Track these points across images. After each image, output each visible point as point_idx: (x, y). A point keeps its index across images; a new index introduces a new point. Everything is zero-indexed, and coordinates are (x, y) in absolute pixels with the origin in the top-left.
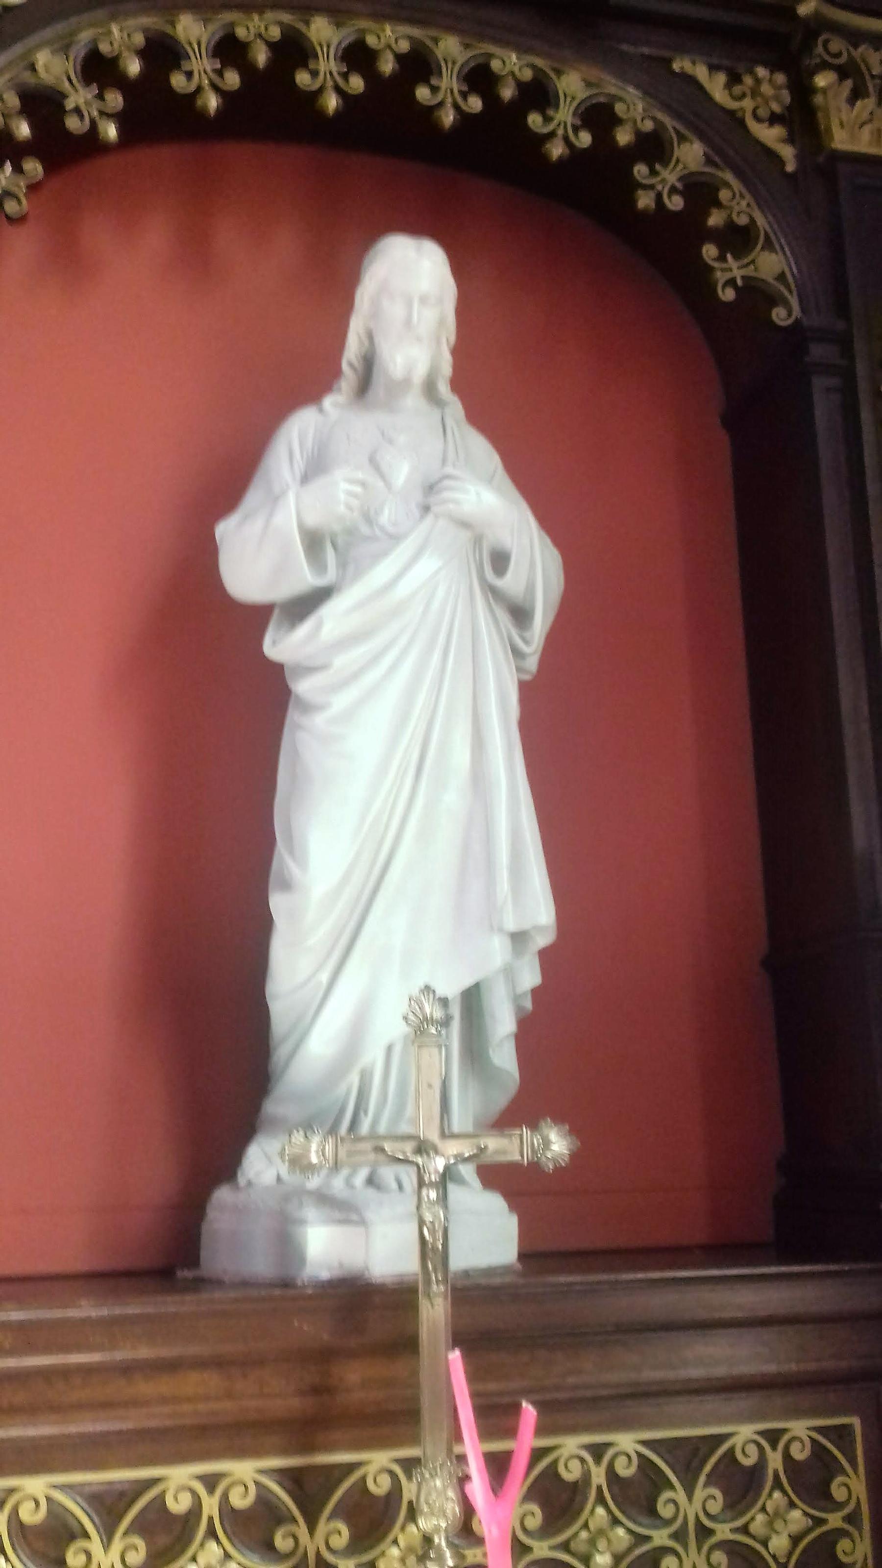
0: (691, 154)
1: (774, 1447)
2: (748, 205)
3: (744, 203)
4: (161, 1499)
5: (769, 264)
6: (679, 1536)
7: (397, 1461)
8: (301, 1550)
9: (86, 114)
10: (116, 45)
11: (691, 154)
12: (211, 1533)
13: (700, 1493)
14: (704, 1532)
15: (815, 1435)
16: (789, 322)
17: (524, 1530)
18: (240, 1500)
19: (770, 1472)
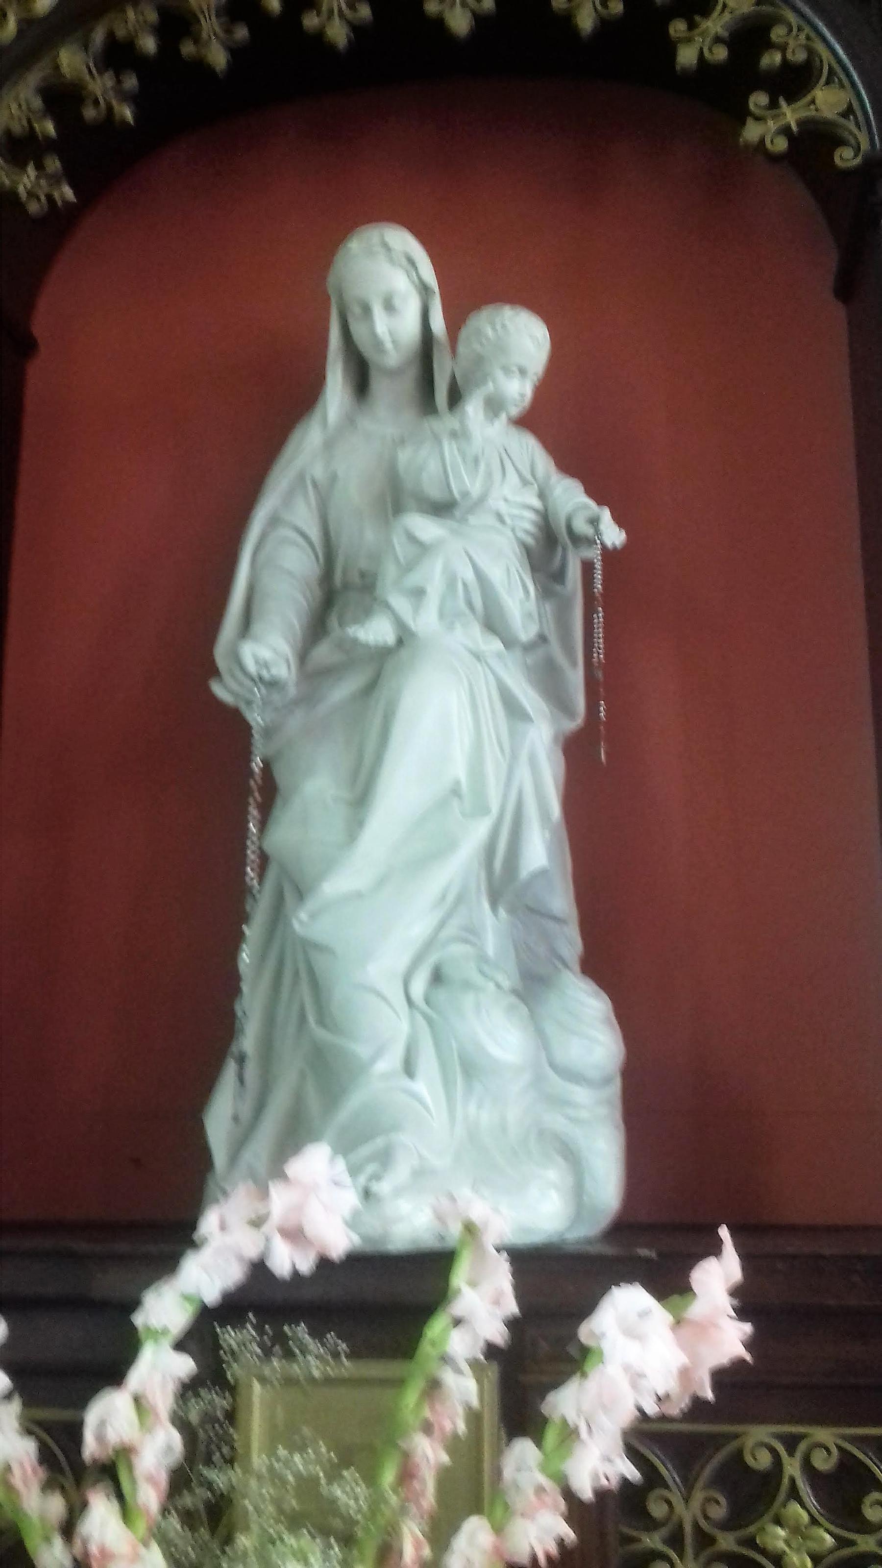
0: (70, 60)
1: (791, 1452)
2: (808, 38)
3: (802, 37)
4: (739, 1455)
5: (826, 101)
6: (676, 1540)
7: (780, 1437)
8: (675, 1518)
9: (101, 101)
10: (130, 26)
11: (70, 60)
12: (794, 1494)
13: (699, 1496)
14: (704, 1540)
15: (840, 1442)
16: (858, 160)
17: (706, 1517)
18: (823, 1462)
19: (786, 1481)
